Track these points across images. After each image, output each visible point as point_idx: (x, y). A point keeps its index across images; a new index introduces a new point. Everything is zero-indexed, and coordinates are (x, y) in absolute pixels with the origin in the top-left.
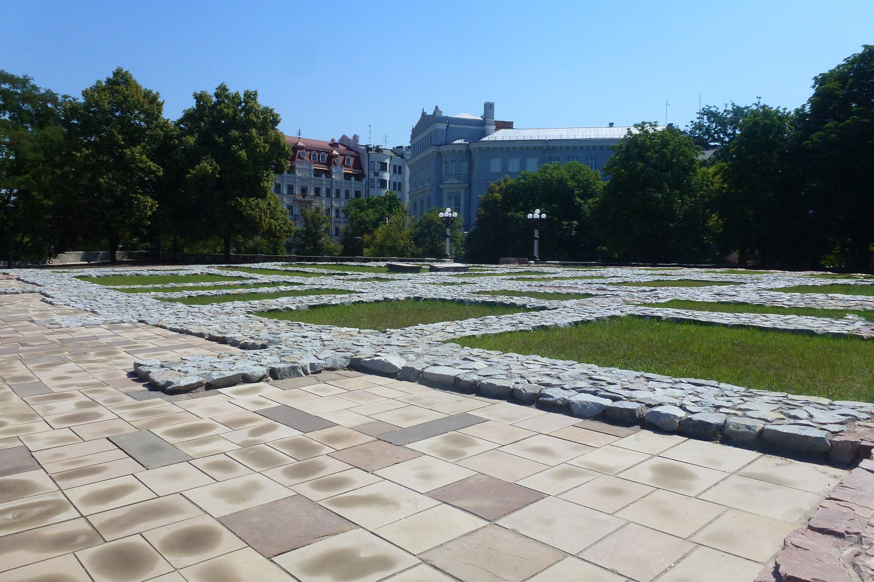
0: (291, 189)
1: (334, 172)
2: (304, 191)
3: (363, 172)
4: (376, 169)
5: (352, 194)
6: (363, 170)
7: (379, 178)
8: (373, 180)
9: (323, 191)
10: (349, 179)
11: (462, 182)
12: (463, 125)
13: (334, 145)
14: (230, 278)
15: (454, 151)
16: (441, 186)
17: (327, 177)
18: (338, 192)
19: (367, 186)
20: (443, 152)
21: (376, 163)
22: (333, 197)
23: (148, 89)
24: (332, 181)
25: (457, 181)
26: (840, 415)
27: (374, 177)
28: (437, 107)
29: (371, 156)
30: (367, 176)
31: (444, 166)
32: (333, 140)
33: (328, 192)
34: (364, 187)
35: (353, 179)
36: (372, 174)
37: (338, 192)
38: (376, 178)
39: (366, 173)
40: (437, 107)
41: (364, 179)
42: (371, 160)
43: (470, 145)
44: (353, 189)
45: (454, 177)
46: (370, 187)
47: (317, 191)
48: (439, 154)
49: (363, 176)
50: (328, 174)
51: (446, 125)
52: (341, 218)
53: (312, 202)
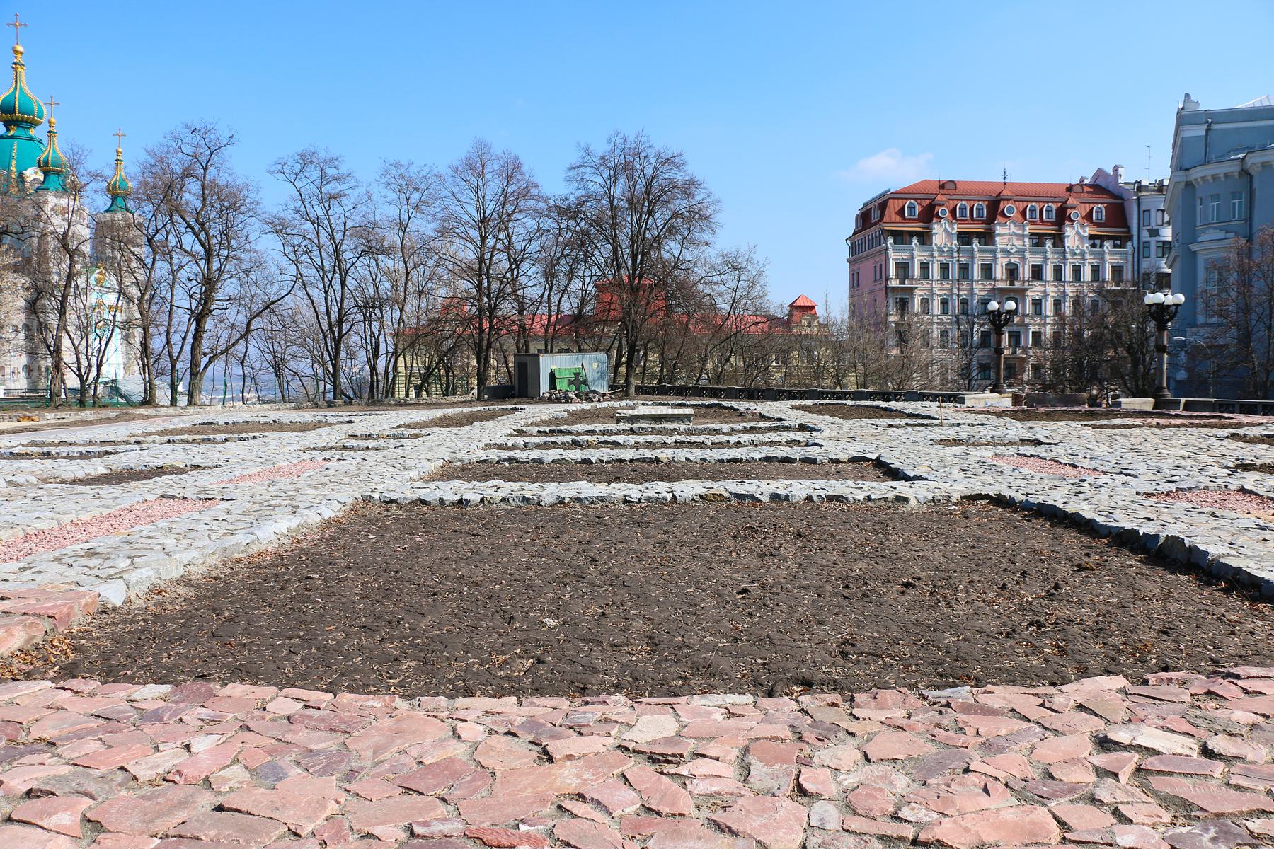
0: (987, 270)
1: (999, 235)
2: (1012, 272)
3: (1129, 231)
4: (1153, 224)
5: (999, 272)
6: (1128, 227)
7: (1157, 238)
8: (1147, 245)
9: (1049, 273)
10: (969, 243)
11: (1232, 235)
12: (1262, 120)
13: (1070, 189)
14: (883, 412)
15: (1214, 177)
16: (1194, 247)
17: (1054, 245)
18: (1077, 270)
19: (1136, 255)
20: (1196, 180)
21: (1153, 212)
22: (976, 278)
23: (513, 154)
24: (1064, 252)
25: (1222, 235)
26: (739, 715)
27: (1149, 239)
28: (1187, 95)
29: (1143, 200)
30: (1135, 238)
31: (1199, 207)
32: (1082, 180)
33: (1058, 271)
34: (1130, 258)
35: (976, 242)
36: (1145, 235)
37: (1077, 270)
38: (1153, 240)
39: (1135, 231)
40: (1187, 95)
41: (1129, 244)
42: (1143, 208)
43: (1247, 159)
44: (1049, 262)
45: (1216, 228)
46: (1141, 256)
47: (1037, 273)
48: (1188, 185)
49: (1130, 238)
50: (925, 237)
51: (1205, 127)
52: (933, 316)
53: (1027, 290)
